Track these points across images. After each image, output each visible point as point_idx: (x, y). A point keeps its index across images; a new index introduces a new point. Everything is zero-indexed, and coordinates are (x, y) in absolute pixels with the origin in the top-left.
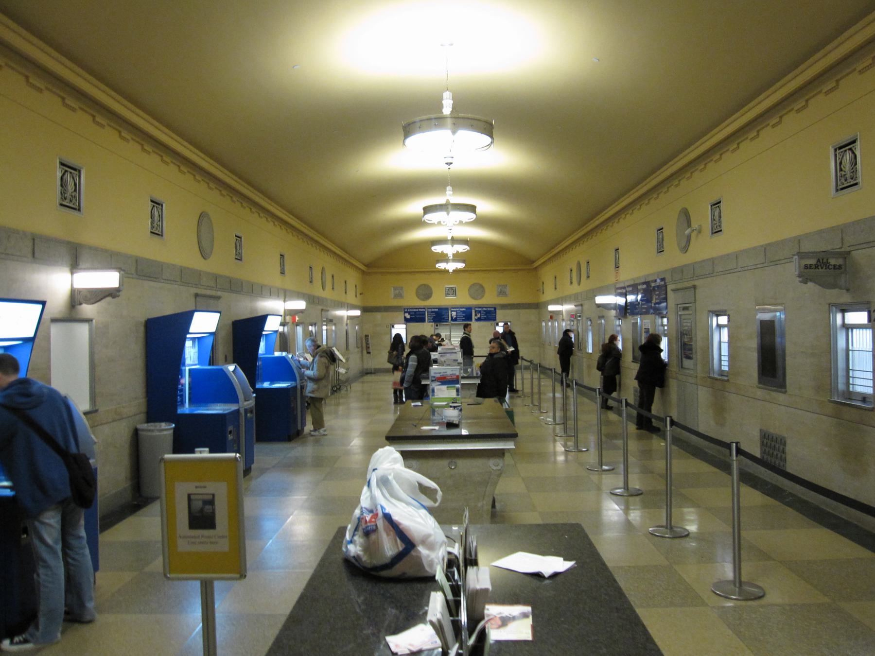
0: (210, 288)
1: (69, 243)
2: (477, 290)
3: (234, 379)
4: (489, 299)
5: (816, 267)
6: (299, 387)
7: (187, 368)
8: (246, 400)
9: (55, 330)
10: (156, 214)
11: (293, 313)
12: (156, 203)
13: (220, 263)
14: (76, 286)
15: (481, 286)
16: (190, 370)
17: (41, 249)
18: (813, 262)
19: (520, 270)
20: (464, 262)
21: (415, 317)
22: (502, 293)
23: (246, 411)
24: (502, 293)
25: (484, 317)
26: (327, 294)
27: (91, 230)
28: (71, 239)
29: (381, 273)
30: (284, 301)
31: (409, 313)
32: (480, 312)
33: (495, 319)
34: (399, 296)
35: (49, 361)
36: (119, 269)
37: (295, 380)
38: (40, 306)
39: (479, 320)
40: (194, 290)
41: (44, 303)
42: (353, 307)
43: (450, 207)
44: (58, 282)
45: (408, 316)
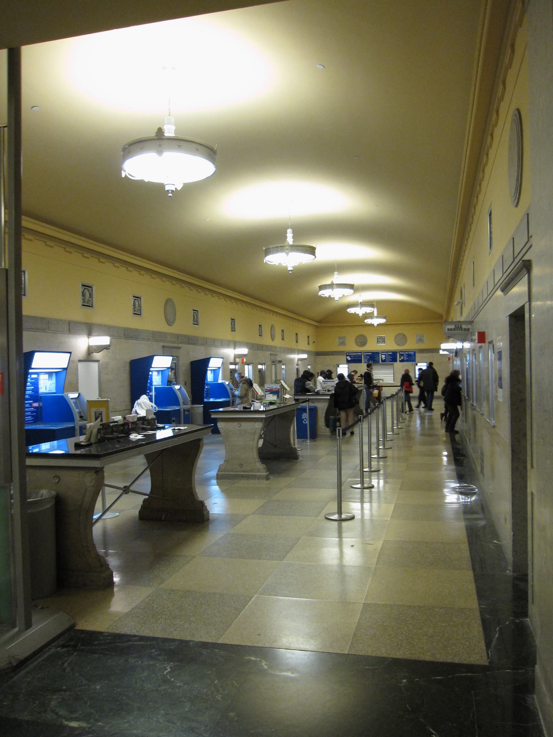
0: (174, 342)
1: (87, 323)
2: (401, 339)
3: (178, 393)
4: (410, 345)
5: (454, 329)
6: (231, 401)
7: (153, 387)
8: (184, 405)
9: (81, 366)
10: (137, 303)
11: (241, 356)
12: (137, 298)
13: (182, 326)
14: (91, 344)
15: (404, 336)
16: (155, 388)
17: (73, 327)
18: (453, 327)
19: (433, 323)
20: (385, 318)
21: (354, 359)
22: (420, 340)
23: (184, 411)
24: (420, 340)
25: (406, 358)
26: (278, 343)
27: (98, 316)
28: (88, 322)
29: (338, 326)
30: (234, 349)
31: (350, 356)
32: (402, 355)
33: (415, 361)
34: (343, 343)
35: (78, 380)
36: (109, 335)
37: (229, 397)
38: (69, 354)
39: (402, 361)
40: (161, 344)
41: (70, 353)
42: (303, 352)
43: (335, 286)
44: (82, 343)
45: (349, 359)
